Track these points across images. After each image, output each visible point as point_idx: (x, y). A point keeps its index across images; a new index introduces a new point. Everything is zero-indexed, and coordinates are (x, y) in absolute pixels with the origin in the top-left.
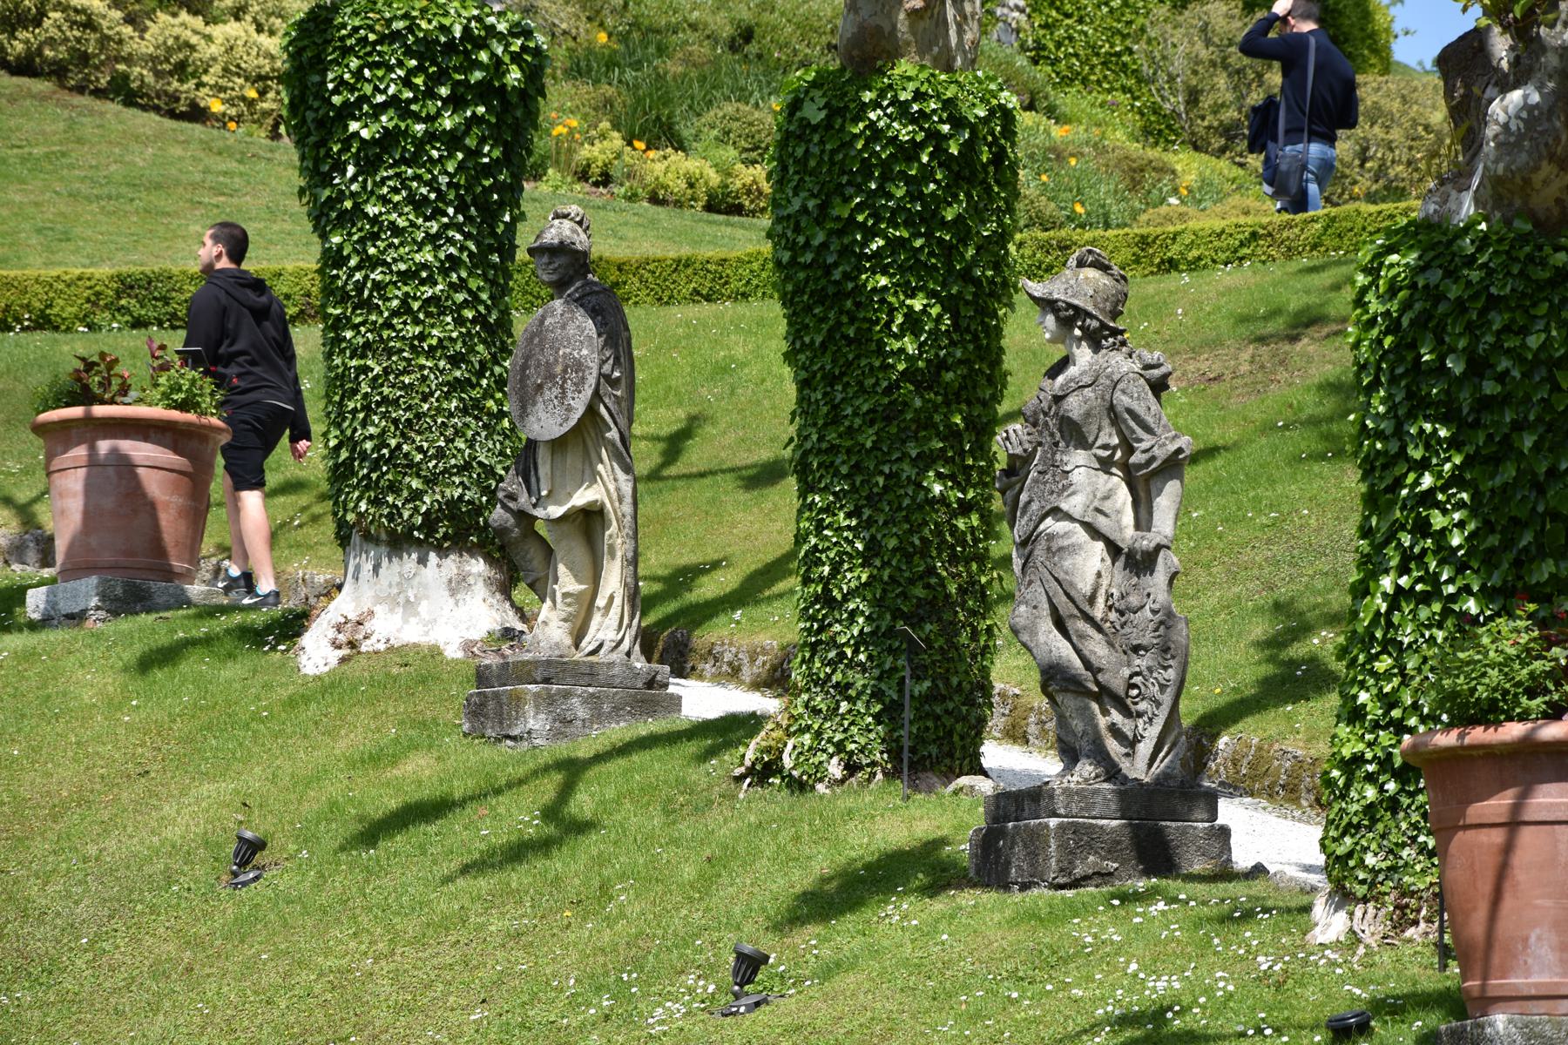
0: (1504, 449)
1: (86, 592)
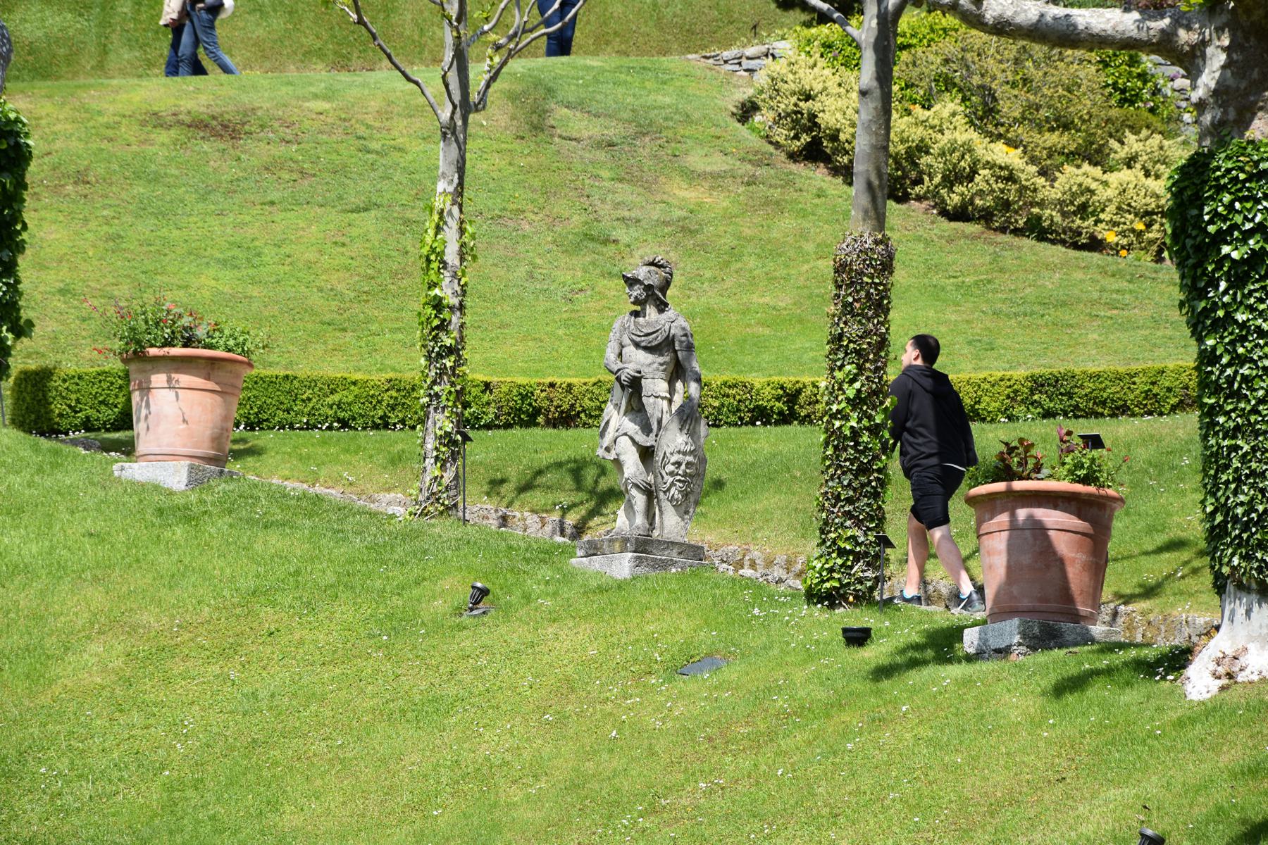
1: (1010, 632)
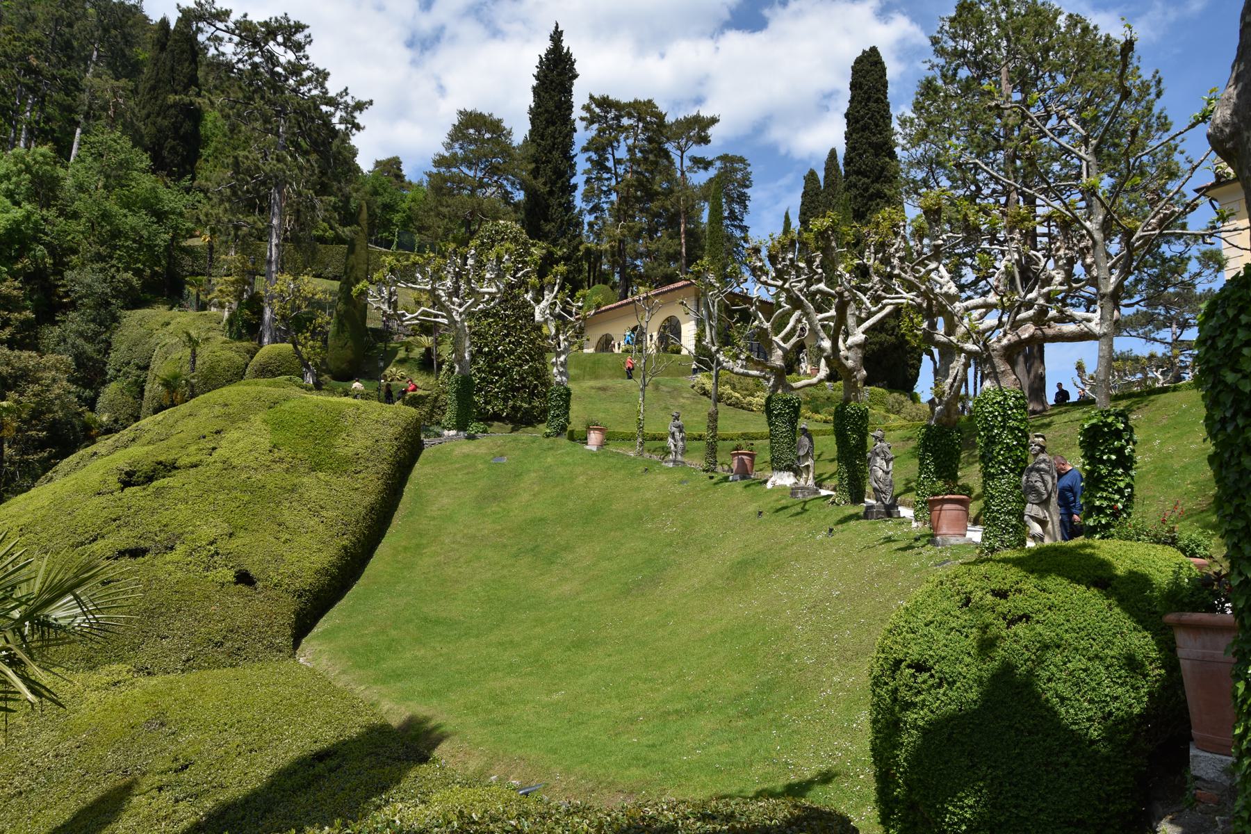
0: (939, 457)
1: (738, 477)
